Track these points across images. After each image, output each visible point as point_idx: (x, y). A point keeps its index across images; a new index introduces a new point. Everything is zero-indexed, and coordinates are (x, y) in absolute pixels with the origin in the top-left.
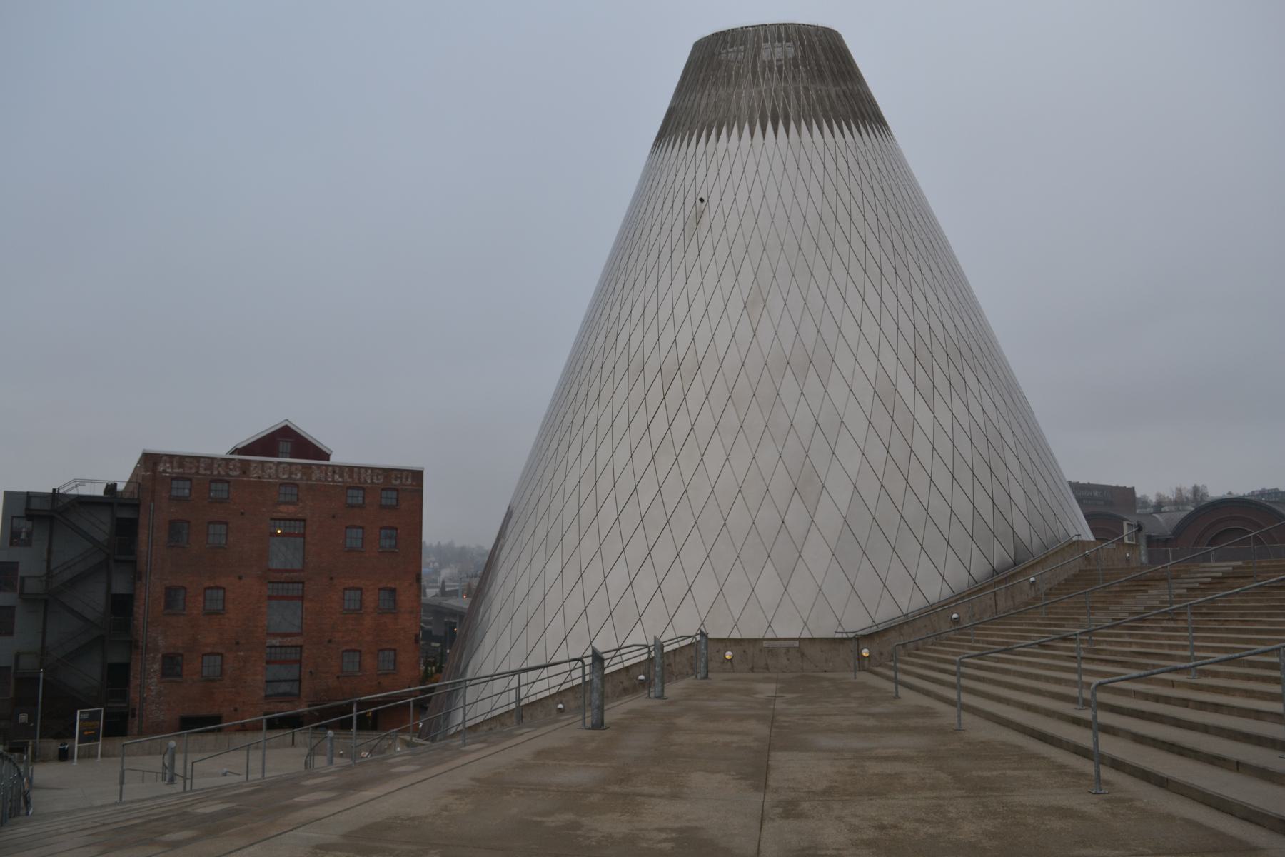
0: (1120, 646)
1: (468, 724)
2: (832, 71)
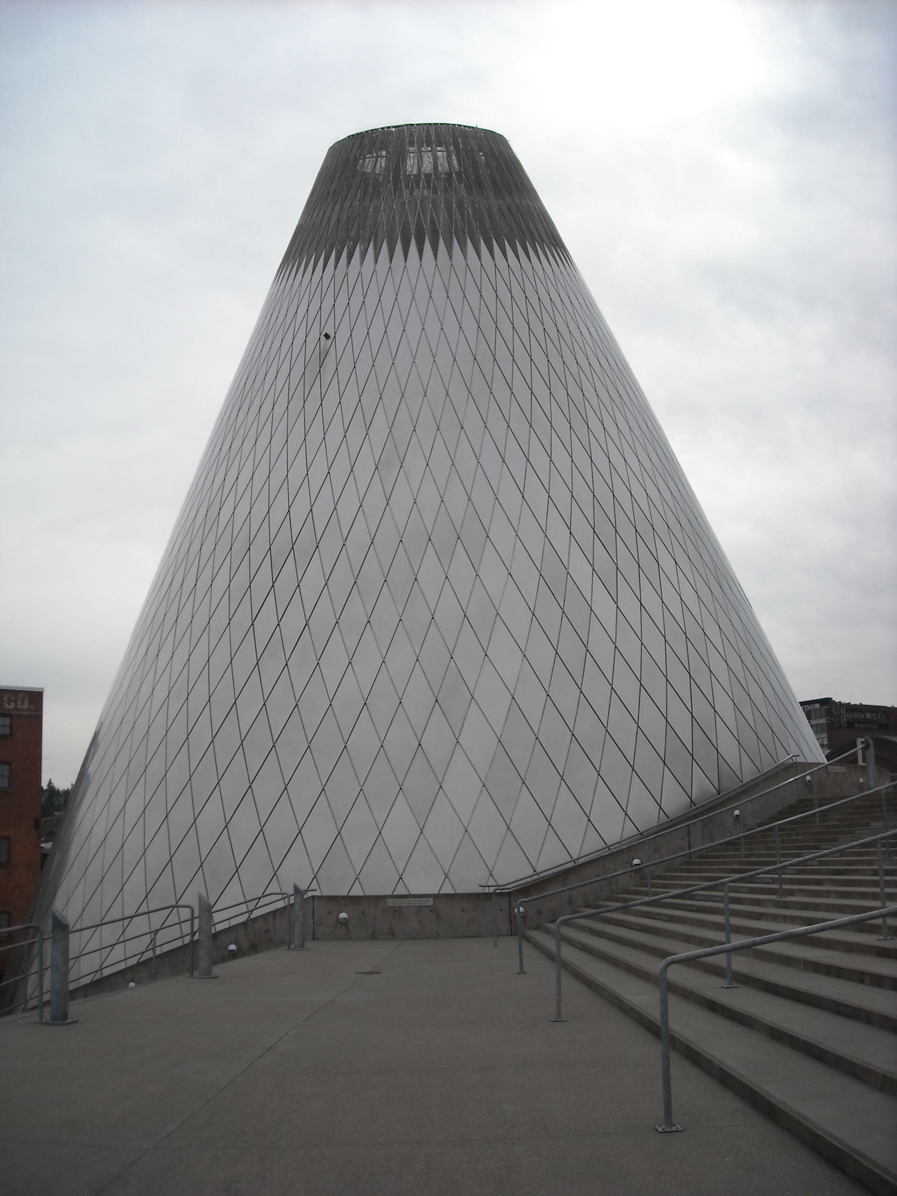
0: (818, 879)
1: (158, 951)
2: (494, 182)
